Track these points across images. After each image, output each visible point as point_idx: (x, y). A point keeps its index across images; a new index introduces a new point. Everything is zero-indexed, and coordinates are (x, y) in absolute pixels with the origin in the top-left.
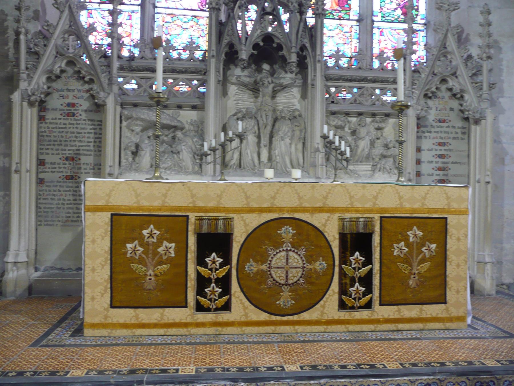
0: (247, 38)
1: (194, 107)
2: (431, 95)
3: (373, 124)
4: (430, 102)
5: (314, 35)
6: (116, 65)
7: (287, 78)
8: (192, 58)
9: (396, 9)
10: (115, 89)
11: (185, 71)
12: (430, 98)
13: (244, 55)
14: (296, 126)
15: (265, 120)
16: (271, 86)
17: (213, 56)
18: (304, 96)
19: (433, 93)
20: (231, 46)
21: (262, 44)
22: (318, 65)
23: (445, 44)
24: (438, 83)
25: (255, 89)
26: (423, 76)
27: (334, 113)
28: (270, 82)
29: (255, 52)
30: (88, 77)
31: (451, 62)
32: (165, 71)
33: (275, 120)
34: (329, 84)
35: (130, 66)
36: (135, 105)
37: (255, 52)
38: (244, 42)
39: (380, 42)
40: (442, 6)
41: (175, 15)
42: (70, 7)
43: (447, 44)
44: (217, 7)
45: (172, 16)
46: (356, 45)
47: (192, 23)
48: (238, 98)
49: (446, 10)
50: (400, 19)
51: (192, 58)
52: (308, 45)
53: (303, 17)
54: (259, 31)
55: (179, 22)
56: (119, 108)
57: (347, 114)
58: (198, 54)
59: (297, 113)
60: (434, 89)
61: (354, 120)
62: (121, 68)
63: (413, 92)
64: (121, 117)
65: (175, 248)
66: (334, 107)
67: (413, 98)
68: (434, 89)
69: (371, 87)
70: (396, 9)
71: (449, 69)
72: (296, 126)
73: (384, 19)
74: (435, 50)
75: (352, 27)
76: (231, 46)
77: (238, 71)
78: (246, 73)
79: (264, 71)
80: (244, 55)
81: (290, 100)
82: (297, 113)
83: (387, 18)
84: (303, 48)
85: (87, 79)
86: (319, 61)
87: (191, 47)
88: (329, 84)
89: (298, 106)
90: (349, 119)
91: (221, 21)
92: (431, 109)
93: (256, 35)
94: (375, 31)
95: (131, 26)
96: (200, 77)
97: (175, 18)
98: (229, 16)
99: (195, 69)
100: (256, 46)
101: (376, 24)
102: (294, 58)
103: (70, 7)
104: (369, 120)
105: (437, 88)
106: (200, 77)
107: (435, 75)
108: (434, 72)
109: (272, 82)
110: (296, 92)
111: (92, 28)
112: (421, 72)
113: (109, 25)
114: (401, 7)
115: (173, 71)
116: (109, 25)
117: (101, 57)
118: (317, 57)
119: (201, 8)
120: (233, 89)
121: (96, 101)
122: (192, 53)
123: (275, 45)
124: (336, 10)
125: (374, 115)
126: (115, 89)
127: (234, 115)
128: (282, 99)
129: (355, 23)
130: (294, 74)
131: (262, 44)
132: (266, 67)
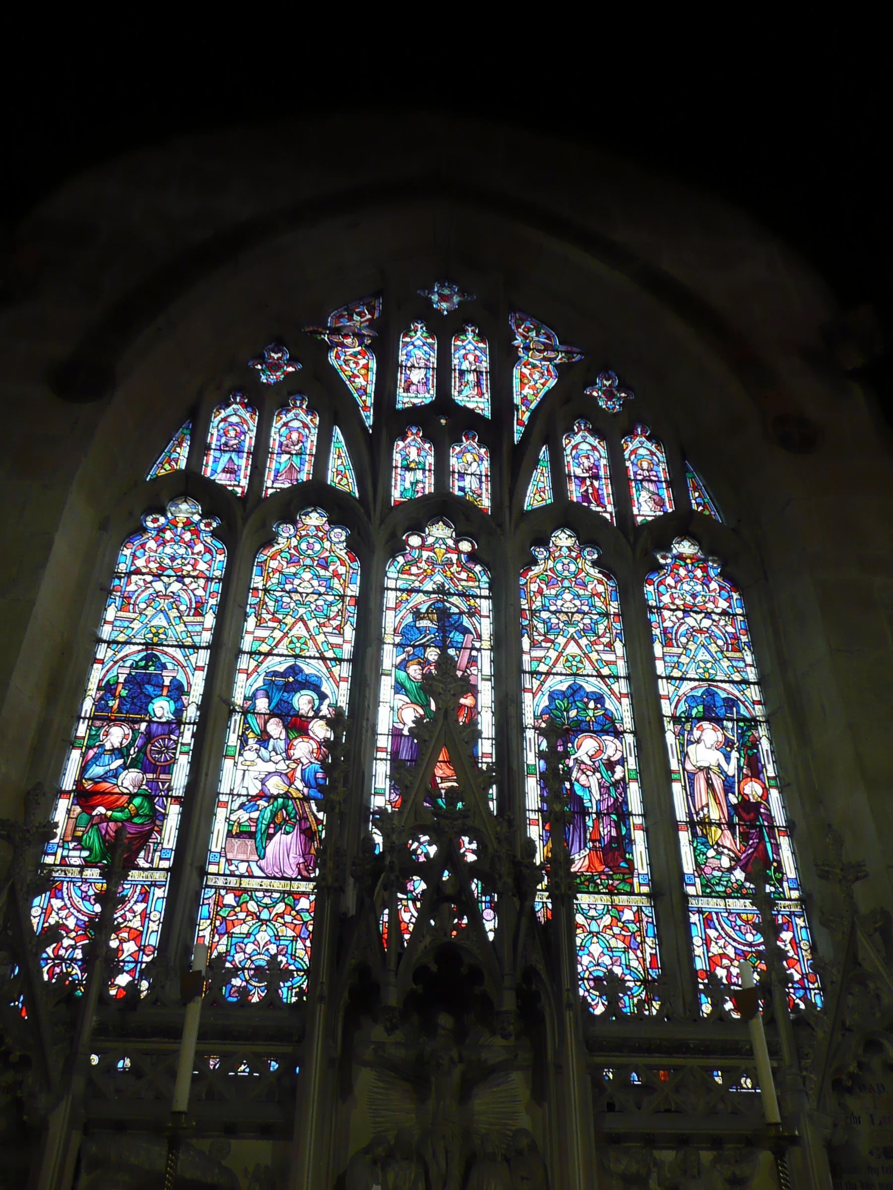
0: (400, 956)
1: (265, 1131)
2: (849, 1084)
3: (718, 1167)
4: (853, 1103)
5: (555, 941)
6: (91, 1020)
7: (494, 1048)
8: (272, 1000)
9: (731, 870)
10: (78, 1083)
11: (252, 1035)
12: (849, 1090)
13: (392, 998)
14: (523, 1178)
15: (443, 1164)
16: (457, 1072)
17: (321, 998)
18: (539, 1094)
19: (851, 1076)
20: (363, 972)
21: (434, 968)
22: (568, 1015)
23: (855, 956)
24: (860, 1052)
25: (417, 1077)
26: (820, 1034)
27: (615, 1139)
28: (456, 1058)
29: (419, 988)
30: (18, 1054)
31: (878, 997)
32: (203, 1036)
33: (470, 1163)
34: (598, 1060)
35: (127, 1020)
36: (120, 1127)
37: (419, 988)
38: (392, 966)
39: (707, 942)
40: (827, 872)
41: (245, 890)
42: (12, 889)
43: (860, 957)
44: (336, 885)
45: (237, 893)
46: (654, 951)
47: (280, 908)
48: (377, 1104)
49: (840, 881)
50: (744, 891)
51: (272, 1000)
52: (540, 967)
53: (527, 903)
54: (428, 939)
55: (252, 906)
56: (77, 1137)
57: (651, 1141)
58: (287, 995)
59: (524, 1142)
60: (853, 1068)
61: (668, 1156)
62: (101, 1031)
63: (804, 1078)
64: (79, 1160)
65: (396, 387)
66: (615, 1124)
67: (807, 1094)
68: (853, 1068)
69: (701, 1067)
70: (731, 870)
71: (878, 1015)
72: (523, 1178)
73: (708, 890)
74: (834, 971)
75: (640, 909)
76: (363, 972)
77: (378, 1033)
78: (398, 1035)
79: (441, 1031)
80: (392, 998)
81: (504, 1104)
82: (524, 1142)
83: (718, 889)
84: (529, 974)
85: (14, 1057)
86: (569, 1006)
87: (272, 973)
88: (598, 1060)
89: (524, 1121)
90: (656, 1153)
91: (345, 914)
92: (858, 1120)
93: (421, 947)
94: (694, 918)
95: (145, 915)
96: (288, 1049)
97: (245, 897)
98: (360, 904)
99: (274, 1027)
100: (421, 973)
101: (693, 903)
102: (509, 1002)
103: (12, 889)
104: (706, 1156)
105: (860, 1065)
106: (288, 1049)
107: (849, 1030)
108: (843, 1023)
109: (461, 1060)
110: (518, 1082)
111: (54, 934)
112: (813, 1024)
113: (100, 898)
114: (741, 864)
115: (226, 1035)
116: (100, 898)
117: (59, 1002)
118: (565, 994)
119: (305, 873)
120: (365, 1079)
121: (25, 1118)
122: (273, 990)
123: (464, 971)
124: (602, 873)
125: (716, 1143)
126: (78, 1083)
127: (367, 1150)
128: (485, 1104)
129: (644, 901)
130: (513, 1038)
131: (434, 968)
132: (445, 1020)
